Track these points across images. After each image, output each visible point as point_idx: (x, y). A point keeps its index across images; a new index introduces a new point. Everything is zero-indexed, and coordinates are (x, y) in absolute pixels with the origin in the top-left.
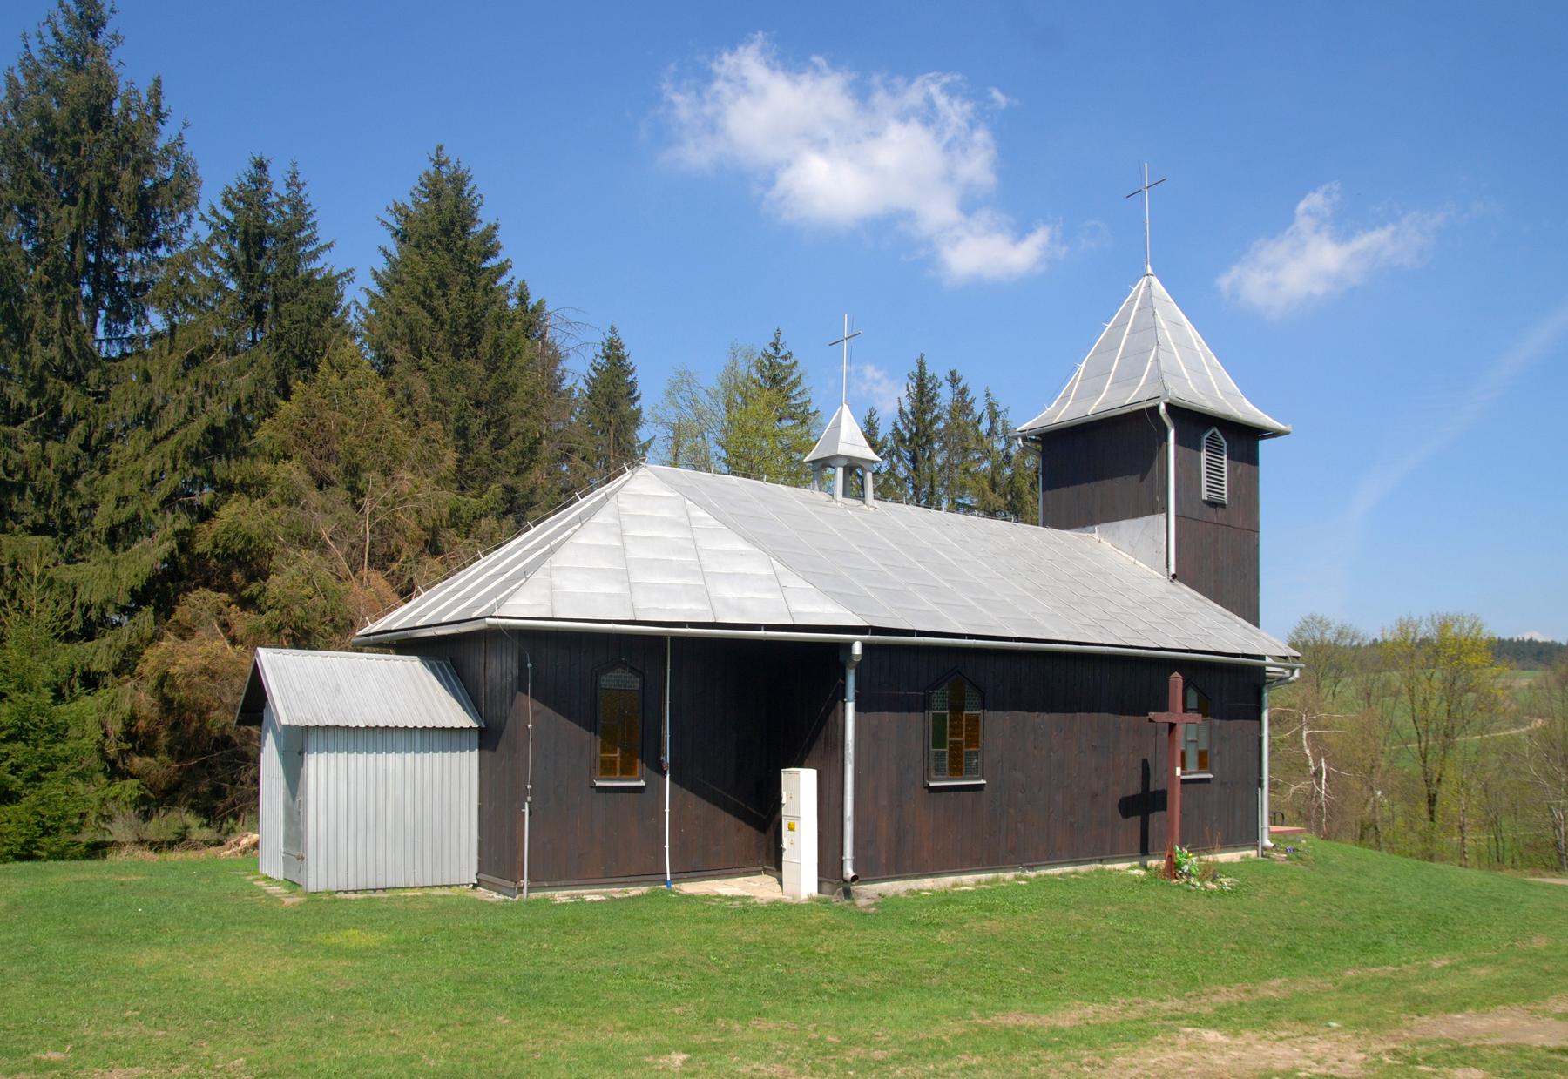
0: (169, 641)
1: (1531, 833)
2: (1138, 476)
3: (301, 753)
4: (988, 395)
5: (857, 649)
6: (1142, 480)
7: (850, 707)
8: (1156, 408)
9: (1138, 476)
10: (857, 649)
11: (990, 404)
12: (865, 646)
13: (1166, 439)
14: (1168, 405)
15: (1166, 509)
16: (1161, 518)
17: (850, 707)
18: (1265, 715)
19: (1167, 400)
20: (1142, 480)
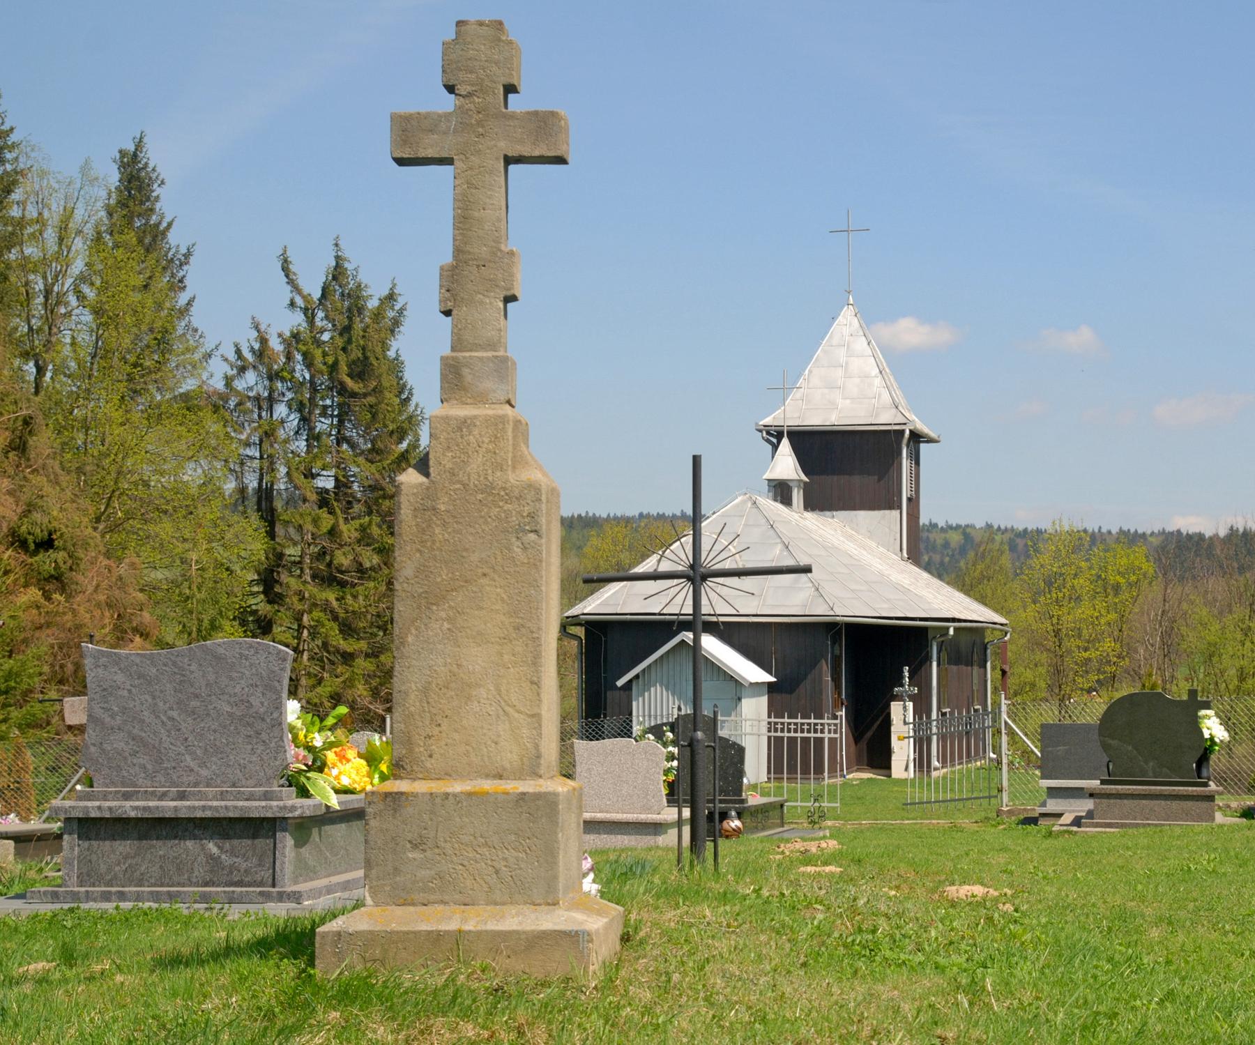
0: (228, 623)
1: (306, 903)
2: (876, 477)
3: (740, 699)
4: (336, 245)
5: (951, 632)
6: (879, 480)
7: (935, 664)
8: (903, 432)
9: (876, 477)
10: (951, 632)
11: (337, 258)
12: (956, 629)
13: (900, 453)
14: (911, 431)
15: (900, 508)
16: (896, 513)
17: (935, 664)
18: (989, 664)
19: (912, 428)
20: (879, 480)
